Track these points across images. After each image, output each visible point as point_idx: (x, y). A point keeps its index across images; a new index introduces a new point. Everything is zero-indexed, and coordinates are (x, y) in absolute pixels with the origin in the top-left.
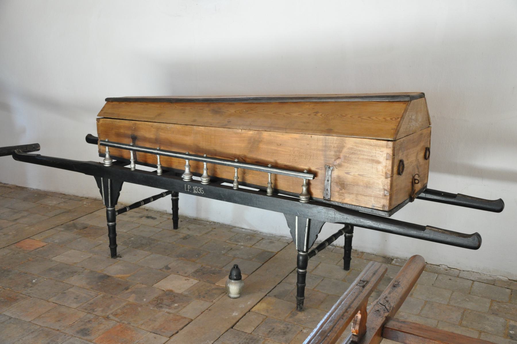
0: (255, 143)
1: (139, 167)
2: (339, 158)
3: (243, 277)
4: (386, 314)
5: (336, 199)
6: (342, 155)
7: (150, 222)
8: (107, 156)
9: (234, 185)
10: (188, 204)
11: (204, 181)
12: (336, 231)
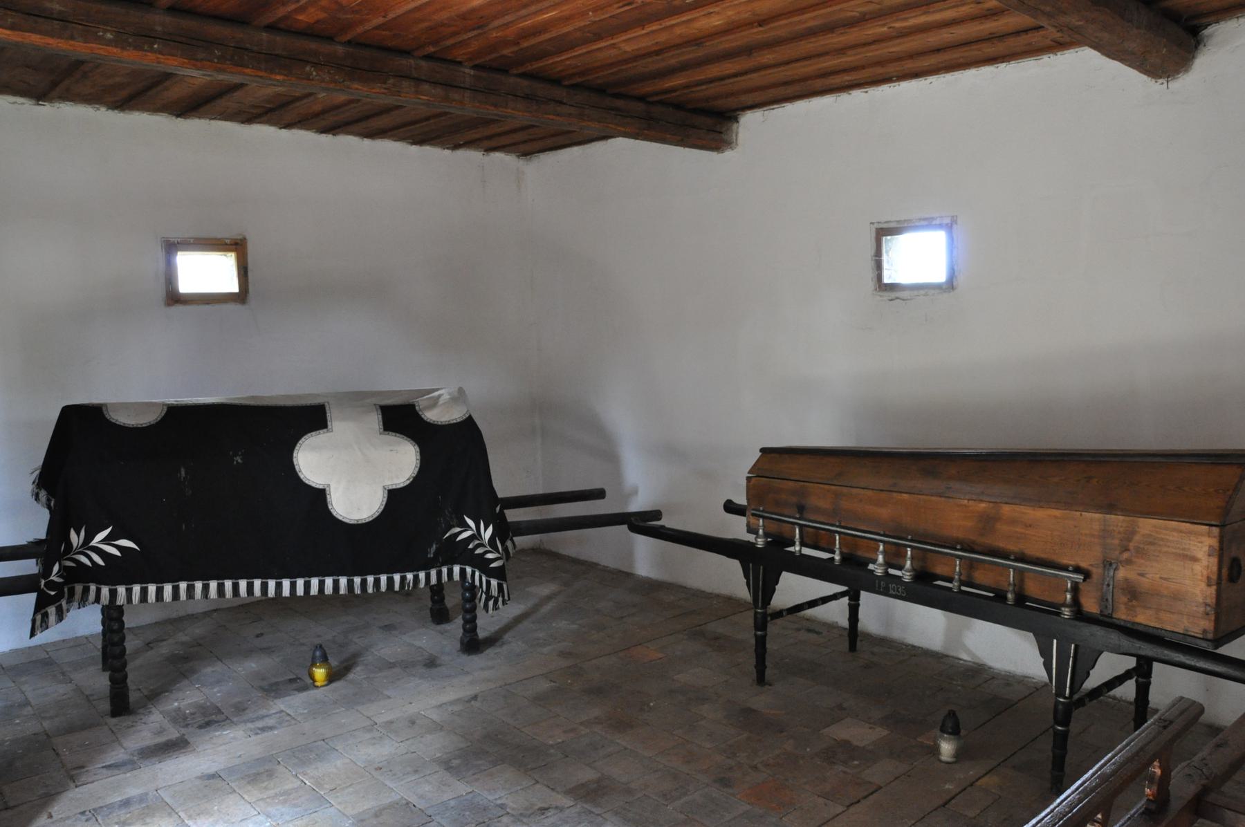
0: (988, 521)
1: (806, 551)
2: (1127, 550)
3: (963, 733)
4: (1204, 782)
5: (1122, 615)
6: (1131, 545)
7: (812, 636)
8: (761, 532)
9: (954, 585)
10: (877, 612)
11: (907, 576)
12: (1121, 672)
